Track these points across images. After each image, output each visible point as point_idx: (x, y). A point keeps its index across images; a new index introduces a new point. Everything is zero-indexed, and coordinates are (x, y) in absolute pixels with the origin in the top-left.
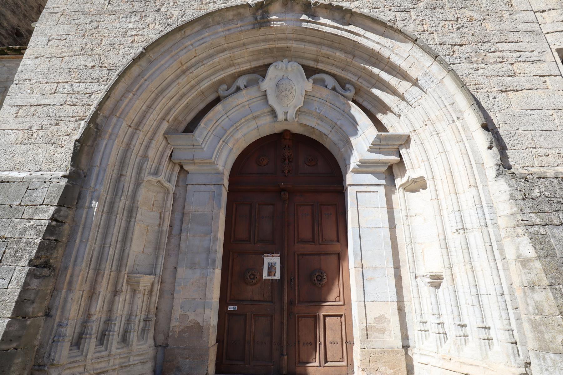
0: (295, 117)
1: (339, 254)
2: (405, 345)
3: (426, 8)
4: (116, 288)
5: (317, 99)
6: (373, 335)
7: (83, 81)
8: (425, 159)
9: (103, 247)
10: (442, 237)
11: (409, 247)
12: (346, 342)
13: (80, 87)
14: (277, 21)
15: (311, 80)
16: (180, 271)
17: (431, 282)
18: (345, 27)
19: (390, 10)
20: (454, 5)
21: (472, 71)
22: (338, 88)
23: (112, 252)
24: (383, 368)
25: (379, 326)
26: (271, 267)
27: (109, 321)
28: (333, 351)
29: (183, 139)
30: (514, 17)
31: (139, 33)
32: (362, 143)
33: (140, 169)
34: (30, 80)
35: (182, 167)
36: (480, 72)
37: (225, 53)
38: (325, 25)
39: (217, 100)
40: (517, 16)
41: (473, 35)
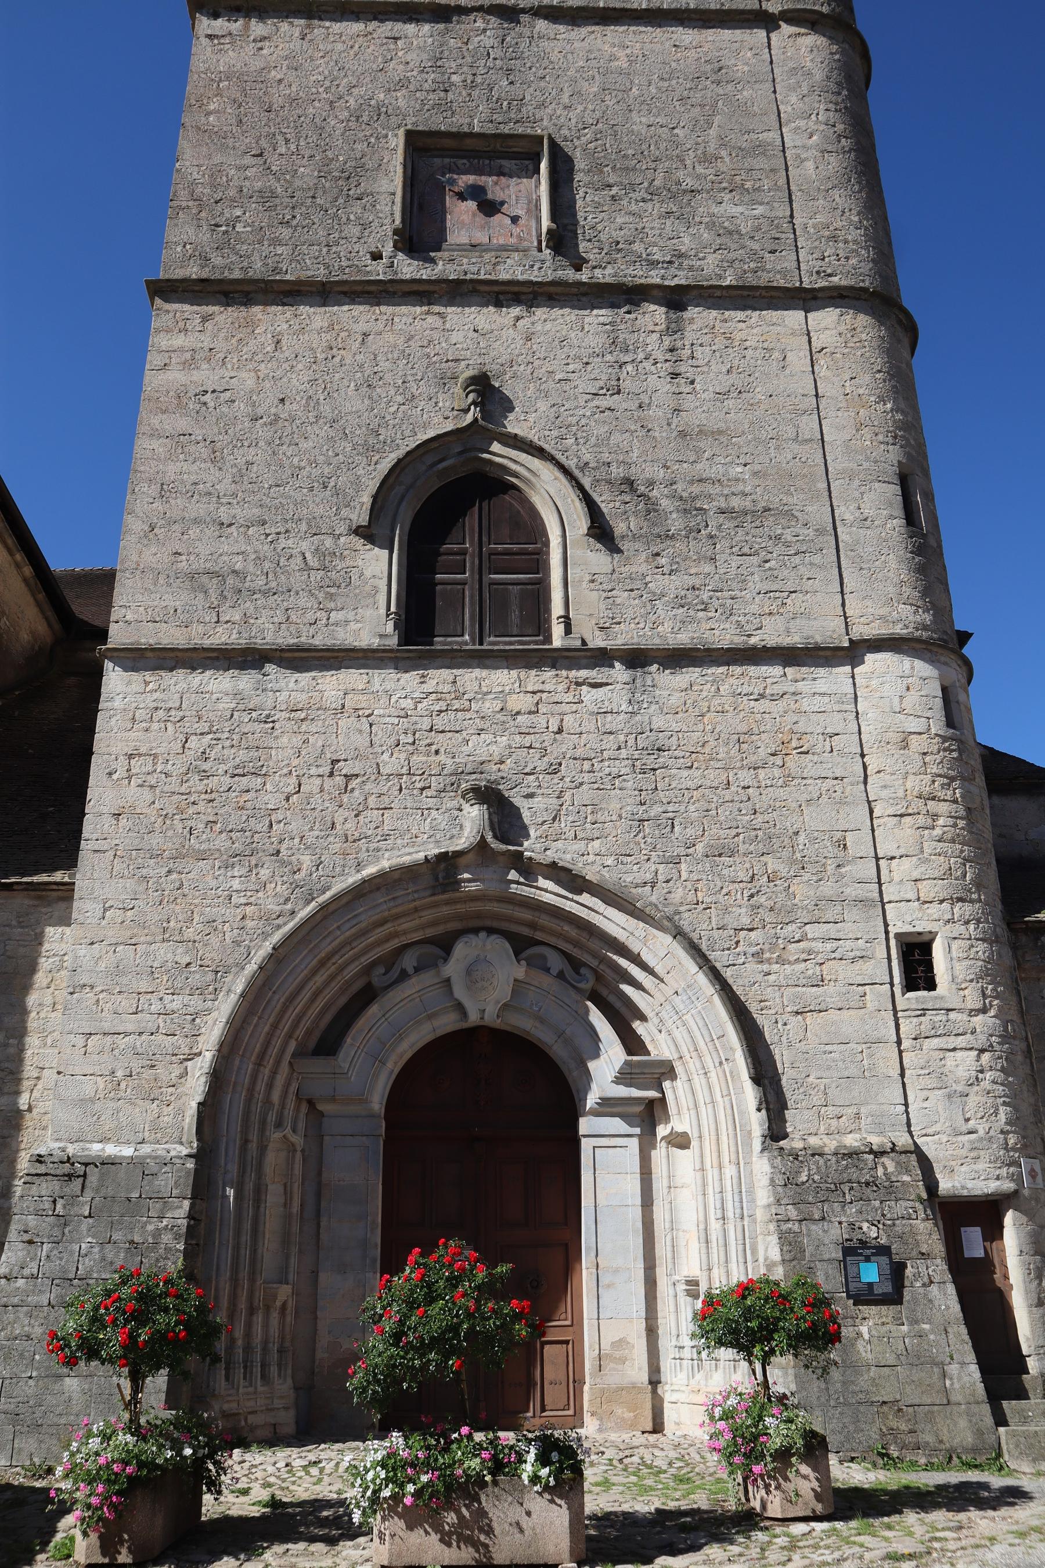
0: (498, 1016)
1: (567, 1245)
2: (654, 1379)
3: (707, 856)
4: (251, 1304)
5: (532, 988)
6: (608, 1366)
7: (177, 991)
8: (691, 1106)
10: (702, 1227)
11: (669, 1237)
12: (574, 1381)
13: (175, 1003)
14: (469, 881)
15: (523, 962)
16: (323, 1277)
17: (686, 1290)
18: (576, 898)
19: (648, 860)
20: (752, 848)
21: (759, 977)
22: (569, 973)
23: (246, 1253)
24: (619, 1411)
25: (617, 1354)
27: (248, 1348)
28: (553, 1395)
29: (318, 1065)
30: (843, 870)
31: (252, 900)
32: (606, 1069)
33: (263, 1123)
34: (92, 987)
36: (772, 978)
37: (386, 927)
38: (546, 891)
40: (847, 868)
41: (771, 909)
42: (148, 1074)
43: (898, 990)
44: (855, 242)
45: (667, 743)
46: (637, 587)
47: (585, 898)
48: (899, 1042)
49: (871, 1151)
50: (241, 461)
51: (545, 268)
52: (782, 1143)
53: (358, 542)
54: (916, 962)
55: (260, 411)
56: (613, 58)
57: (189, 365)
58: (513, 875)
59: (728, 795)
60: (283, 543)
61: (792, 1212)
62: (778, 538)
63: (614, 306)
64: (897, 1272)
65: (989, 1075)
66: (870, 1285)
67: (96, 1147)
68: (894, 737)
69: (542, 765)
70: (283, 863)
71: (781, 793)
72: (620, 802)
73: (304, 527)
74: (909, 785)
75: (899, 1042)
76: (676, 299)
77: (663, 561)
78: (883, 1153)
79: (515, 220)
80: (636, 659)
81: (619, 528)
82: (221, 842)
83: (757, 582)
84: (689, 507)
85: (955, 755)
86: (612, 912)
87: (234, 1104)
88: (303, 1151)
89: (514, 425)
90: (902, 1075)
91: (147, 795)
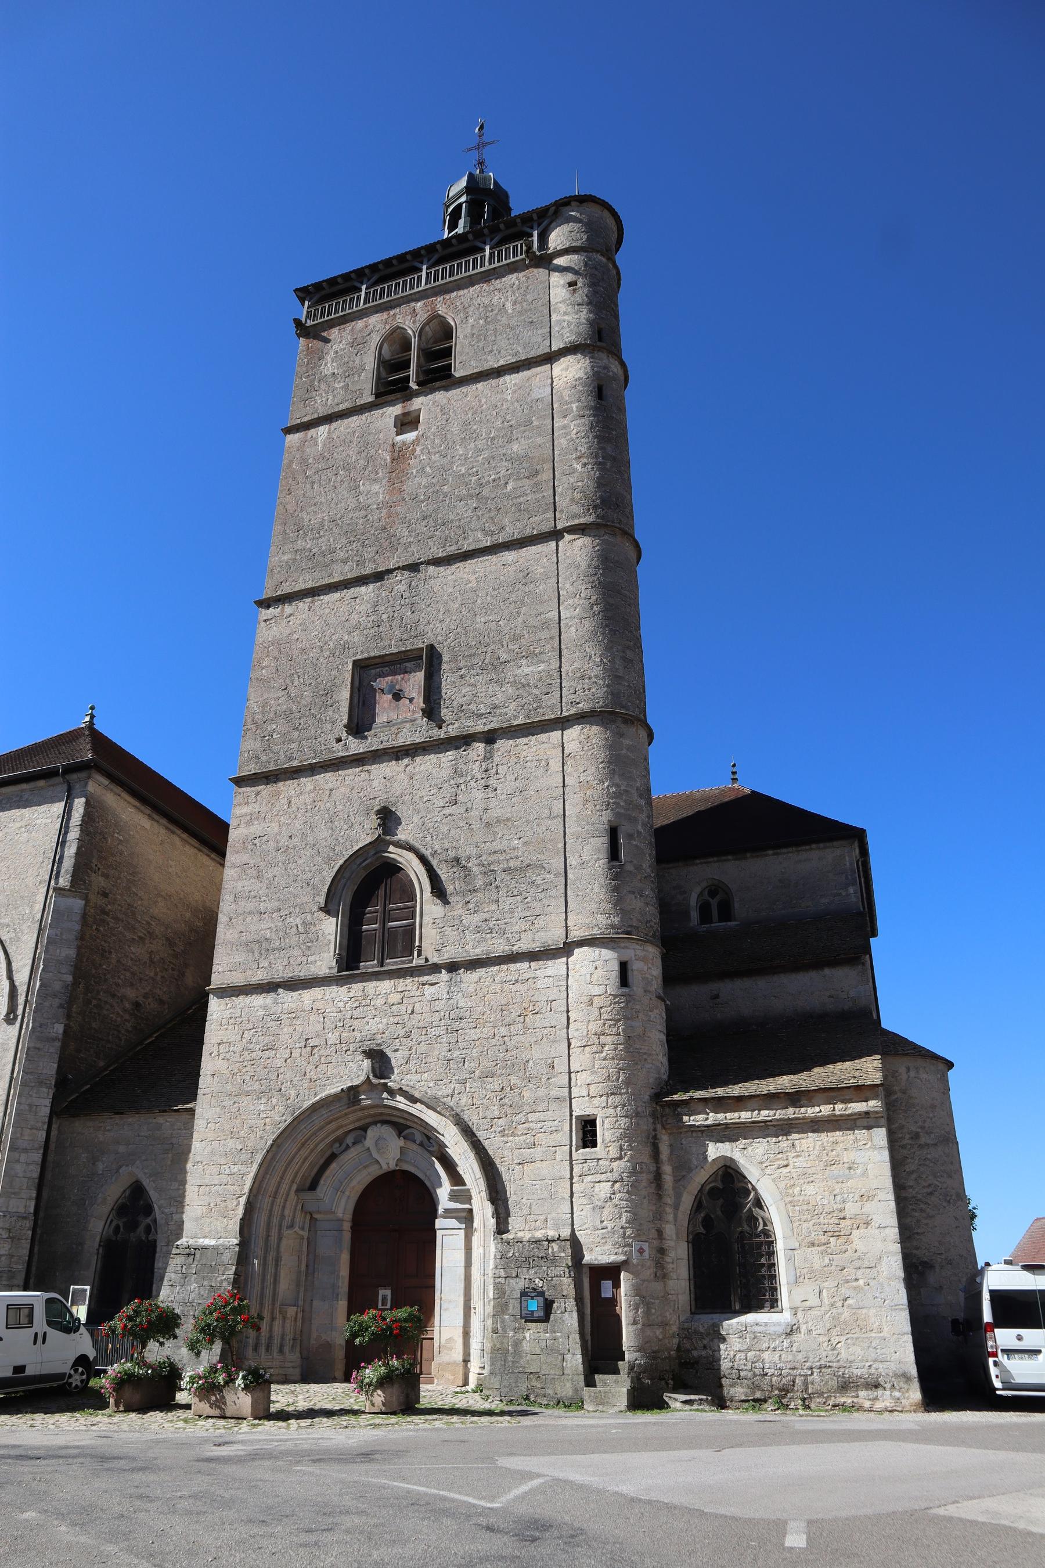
6: (444, 1352)
9: (263, 1288)
21: (502, 1145)
23: (268, 1292)
24: (447, 1375)
25: (448, 1345)
26: (384, 1298)
27: (271, 1337)
29: (309, 1196)
33: (280, 1226)
35: (311, 1217)
39: (333, 1157)
42: (223, 1204)
43: (574, 1149)
44: (596, 676)
45: (465, 1014)
46: (458, 925)
47: (418, 1105)
48: (572, 1178)
49: (547, 1240)
50: (271, 875)
51: (420, 731)
52: (504, 1236)
53: (322, 915)
54: (587, 1132)
55: (280, 844)
56: (469, 581)
57: (249, 823)
58: (385, 1095)
59: (493, 1042)
60: (288, 920)
61: (502, 1273)
62: (533, 882)
63: (457, 748)
64: (548, 1306)
65: (618, 1196)
66: (533, 1312)
67: (202, 1240)
68: (585, 999)
69: (402, 1033)
70: (283, 1095)
71: (521, 1038)
72: (440, 1050)
73: (298, 910)
74: (590, 1027)
75: (572, 1178)
76: (490, 738)
77: (471, 906)
78: (554, 1241)
79: (411, 700)
80: (452, 967)
81: (450, 888)
82: (256, 1086)
83: (520, 913)
84: (488, 871)
85: (622, 1005)
86: (430, 1112)
87: (260, 1220)
88: (308, 1238)
89: (402, 834)
90: (572, 1196)
91: (225, 1064)
